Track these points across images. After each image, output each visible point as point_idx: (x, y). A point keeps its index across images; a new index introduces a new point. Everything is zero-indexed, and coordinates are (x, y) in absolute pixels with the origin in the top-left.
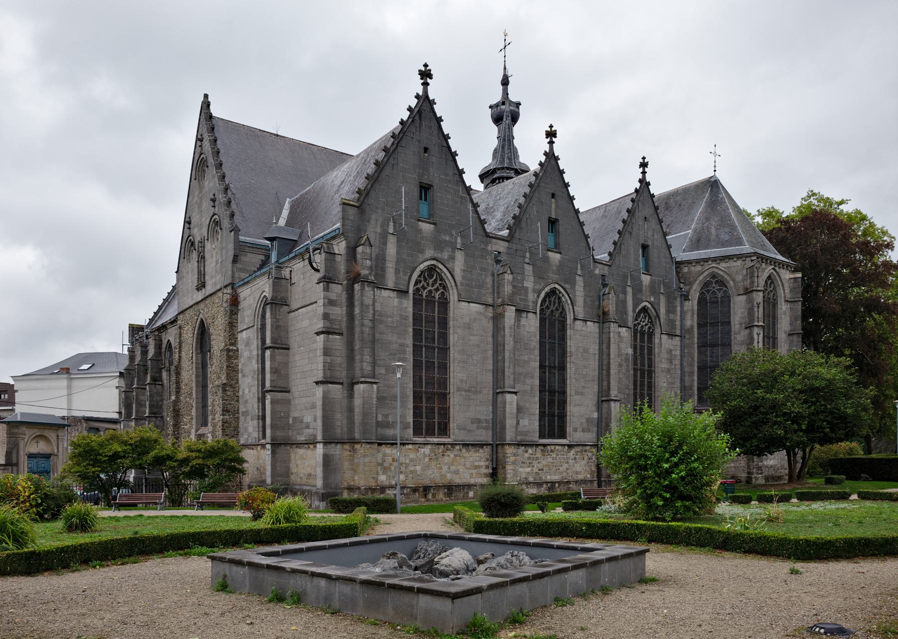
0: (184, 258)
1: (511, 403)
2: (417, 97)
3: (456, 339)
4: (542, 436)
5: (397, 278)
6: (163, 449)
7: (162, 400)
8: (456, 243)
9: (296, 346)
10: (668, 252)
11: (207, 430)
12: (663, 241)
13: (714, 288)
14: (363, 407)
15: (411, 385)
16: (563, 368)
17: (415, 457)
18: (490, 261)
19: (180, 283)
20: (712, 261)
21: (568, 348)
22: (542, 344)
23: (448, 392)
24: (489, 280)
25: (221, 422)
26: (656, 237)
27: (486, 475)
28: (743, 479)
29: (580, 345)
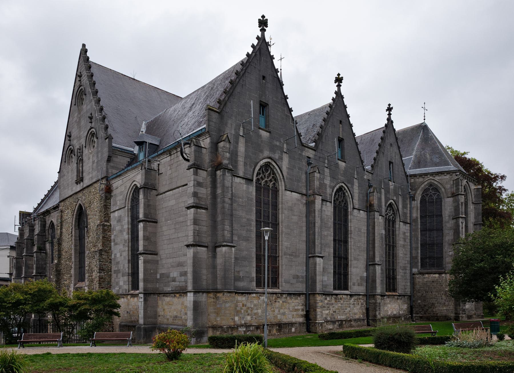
0: (65, 162)
1: (320, 265)
2: (258, 38)
3: (283, 218)
4: (335, 289)
5: (245, 169)
6: (56, 297)
7: (46, 264)
8: (283, 147)
9: (163, 220)
10: (403, 168)
11: (85, 286)
12: (400, 161)
13: (431, 193)
14: (225, 265)
15: (254, 250)
16: (346, 242)
17: (257, 303)
18: (304, 163)
19: (62, 180)
20: (430, 175)
21: (349, 228)
22: (335, 224)
23: (278, 255)
24: (304, 177)
25: (98, 278)
26: (396, 157)
27: (302, 316)
28: (452, 318)
29: (356, 226)
